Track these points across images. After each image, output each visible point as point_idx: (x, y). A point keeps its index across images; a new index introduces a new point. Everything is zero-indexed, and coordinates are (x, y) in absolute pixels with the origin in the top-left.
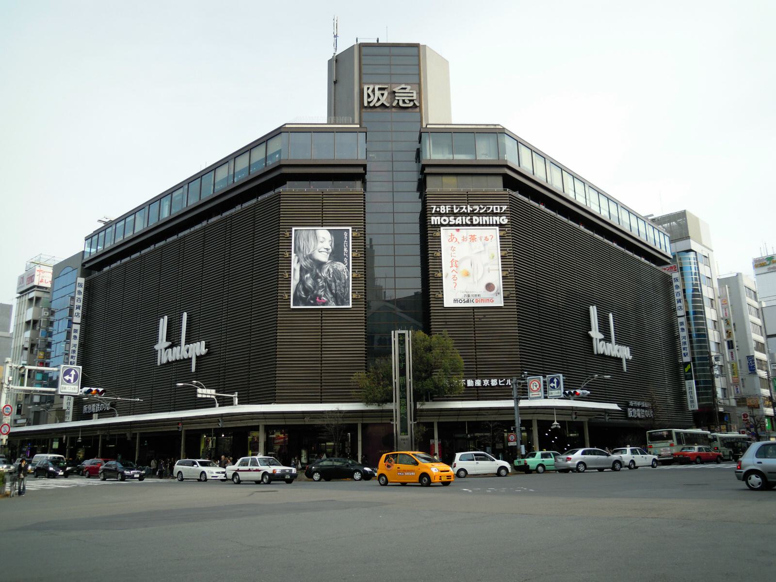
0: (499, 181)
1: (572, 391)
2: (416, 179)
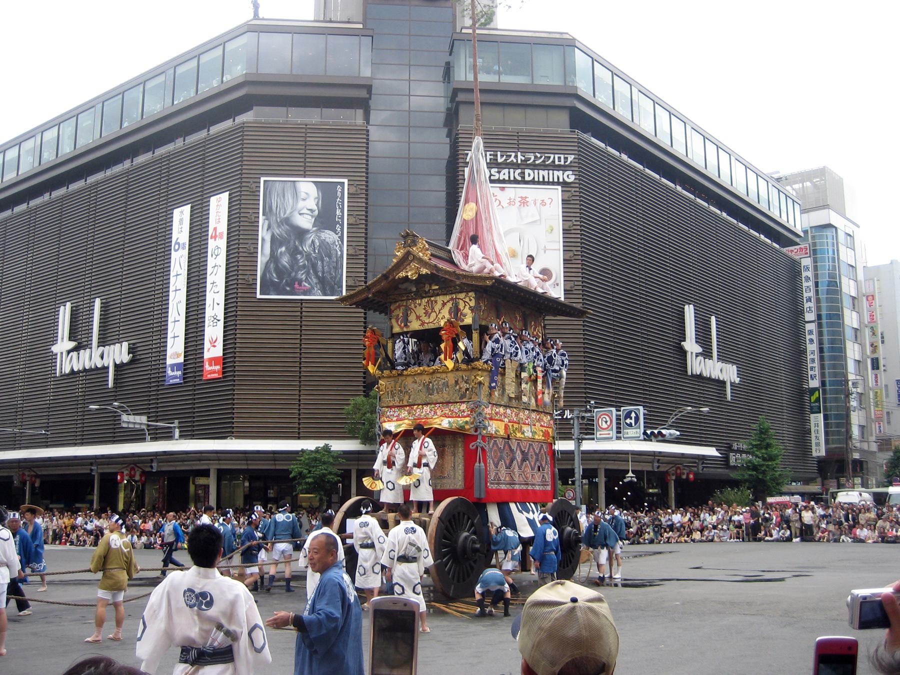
0: (563, 118)
1: (656, 431)
2: (443, 109)
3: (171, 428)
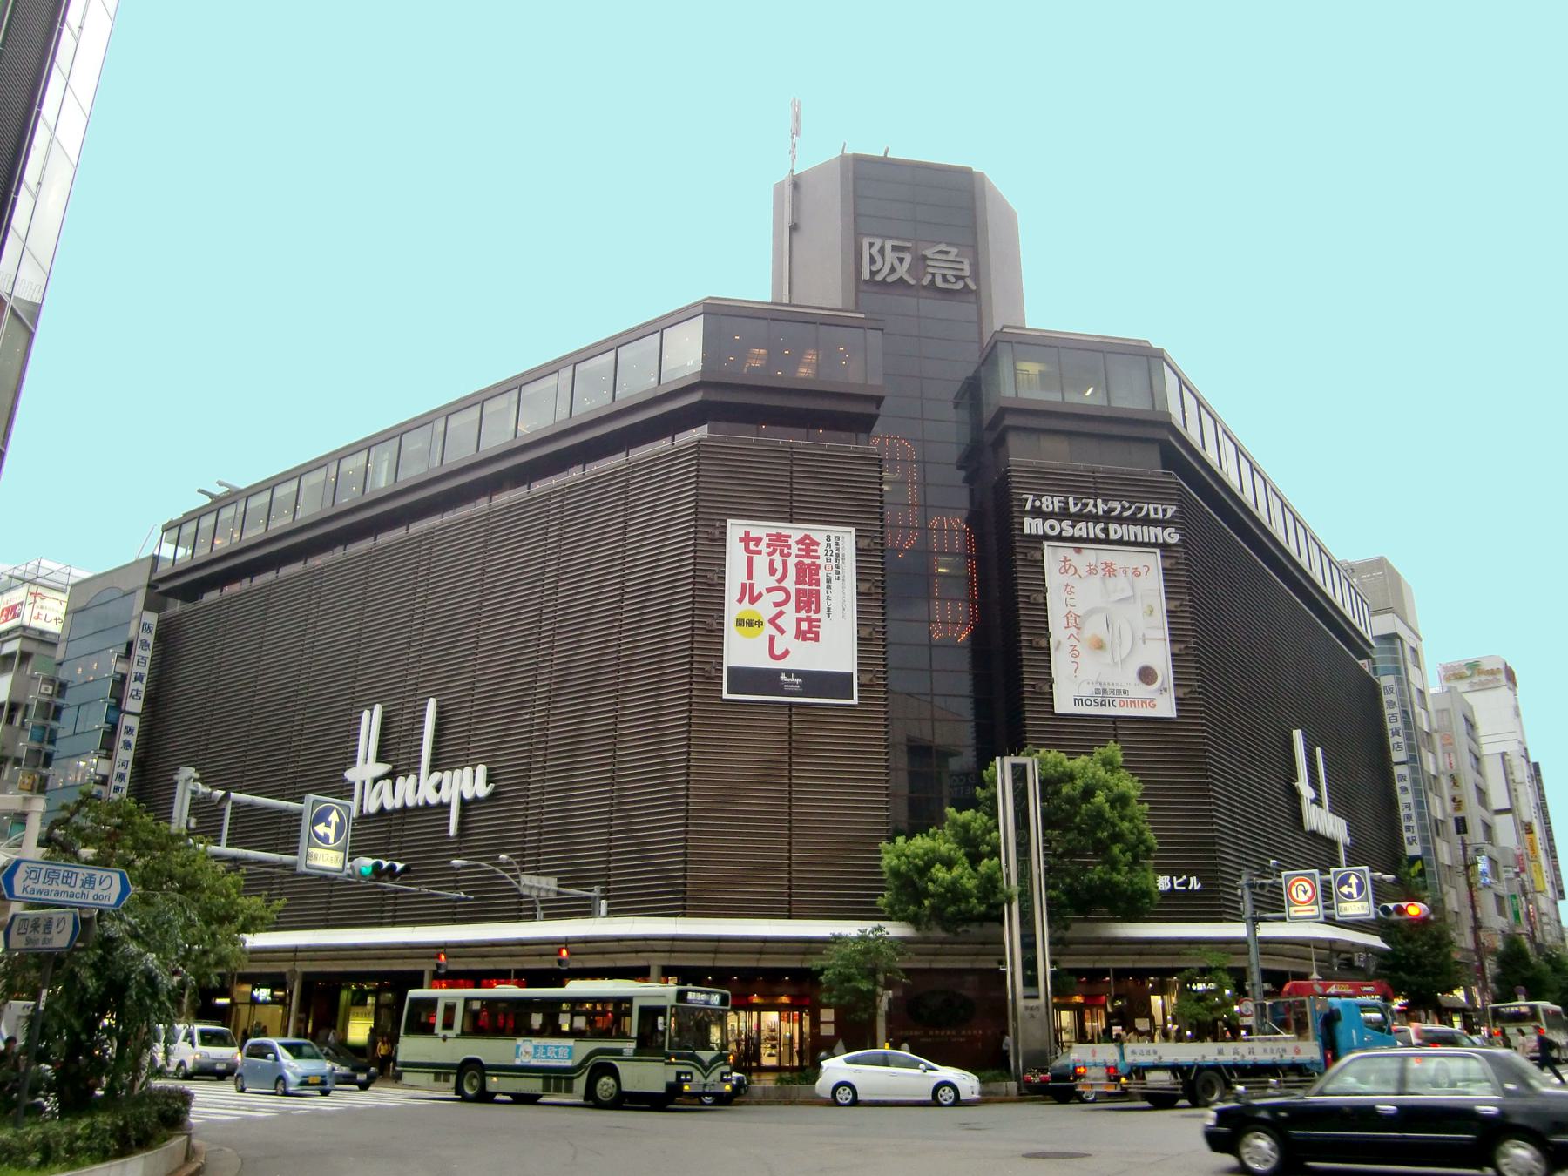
3: (588, 898)
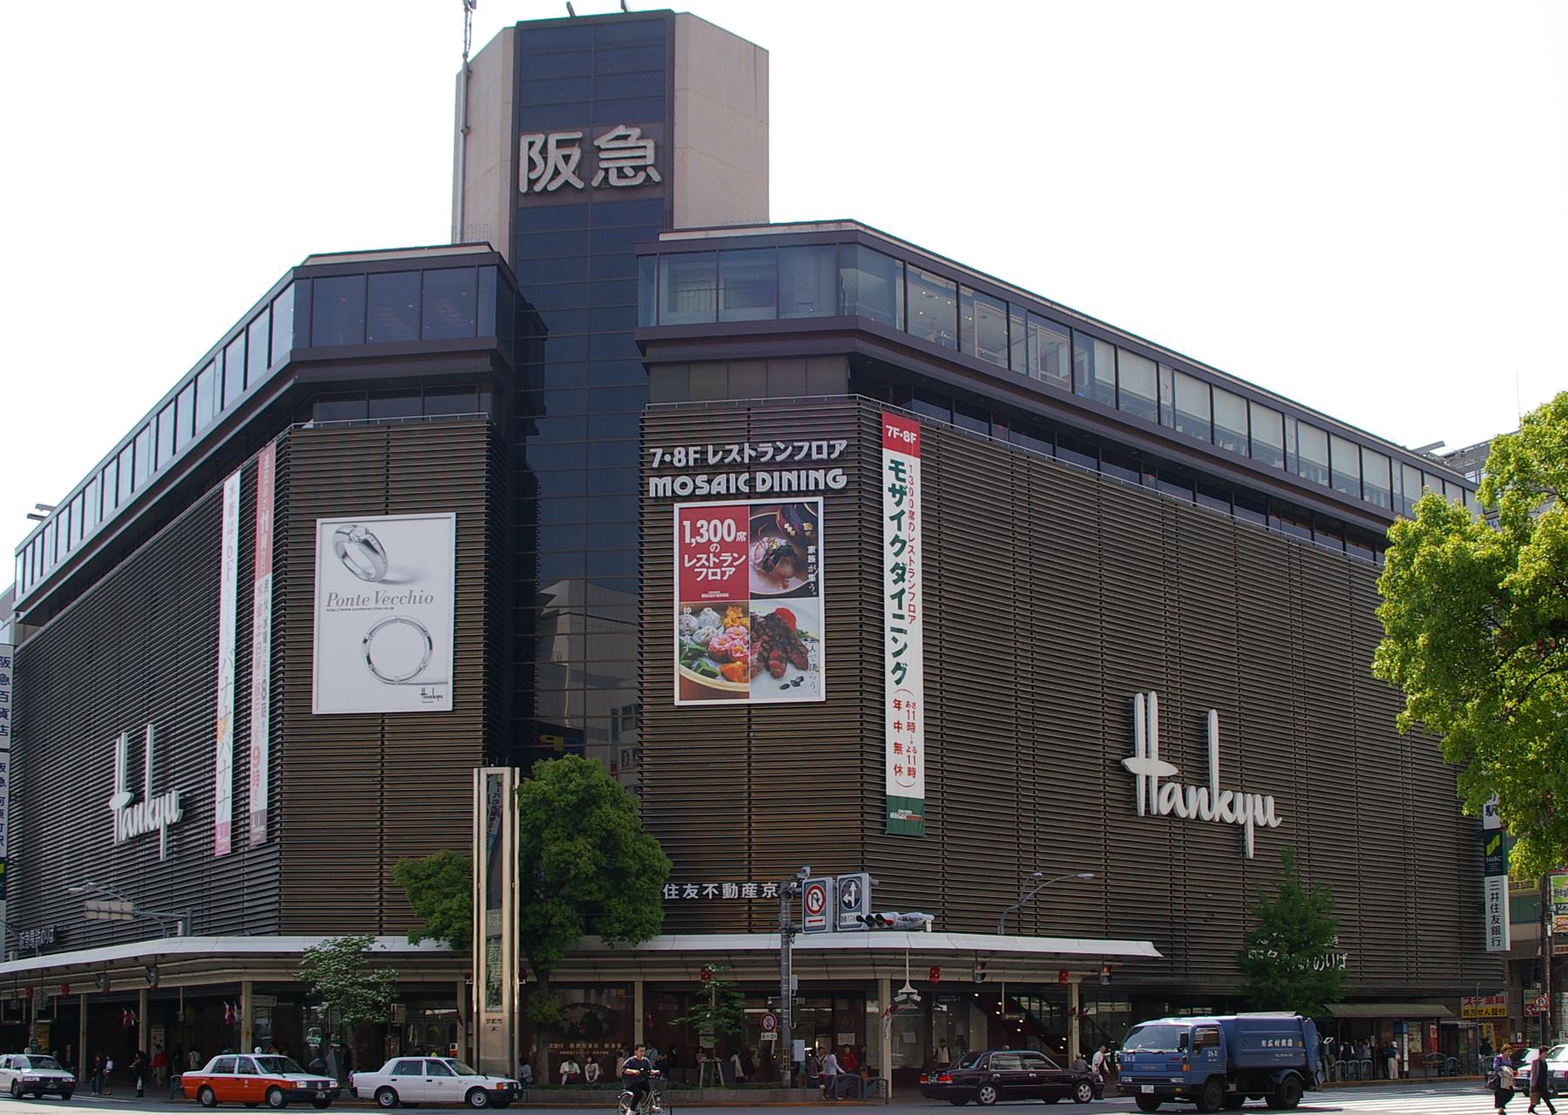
0: (839, 373)
